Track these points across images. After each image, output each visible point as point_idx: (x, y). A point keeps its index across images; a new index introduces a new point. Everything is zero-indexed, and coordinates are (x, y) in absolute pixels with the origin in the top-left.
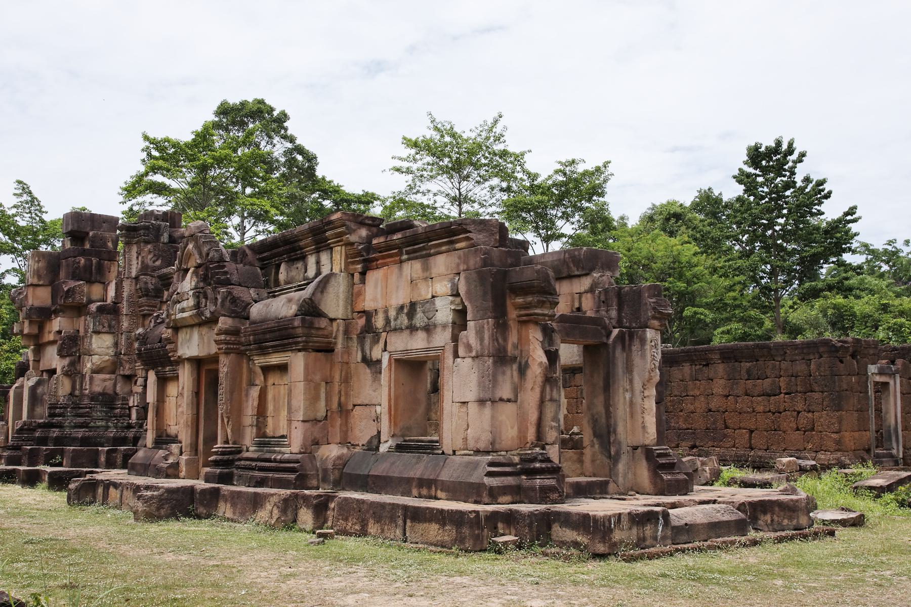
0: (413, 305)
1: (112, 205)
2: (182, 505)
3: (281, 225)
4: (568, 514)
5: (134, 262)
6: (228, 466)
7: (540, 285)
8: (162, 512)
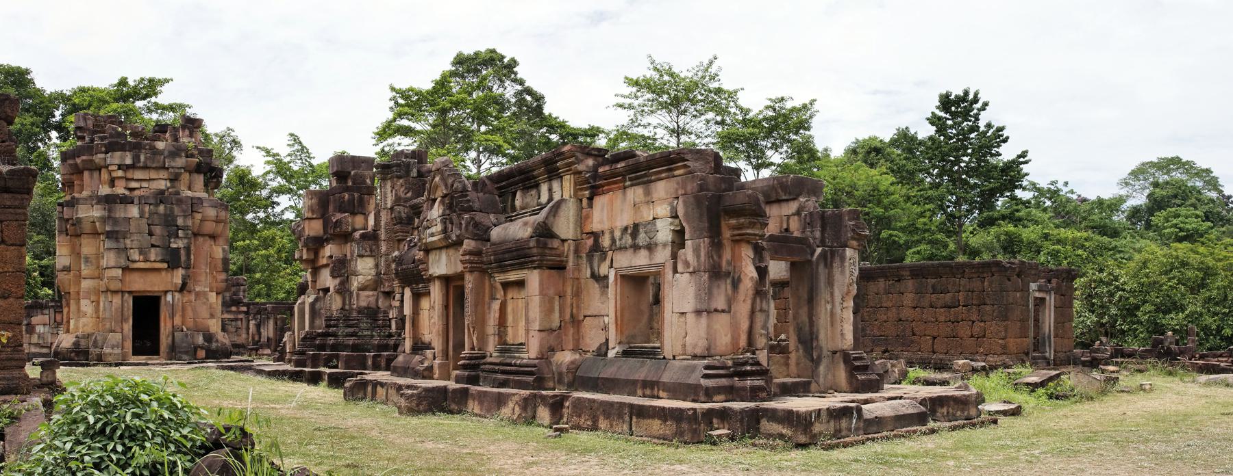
0: (636, 226)
1: (366, 147)
2: (437, 402)
3: (513, 158)
4: (774, 411)
5: (389, 195)
6: (475, 369)
7: (752, 208)
8: (421, 407)
